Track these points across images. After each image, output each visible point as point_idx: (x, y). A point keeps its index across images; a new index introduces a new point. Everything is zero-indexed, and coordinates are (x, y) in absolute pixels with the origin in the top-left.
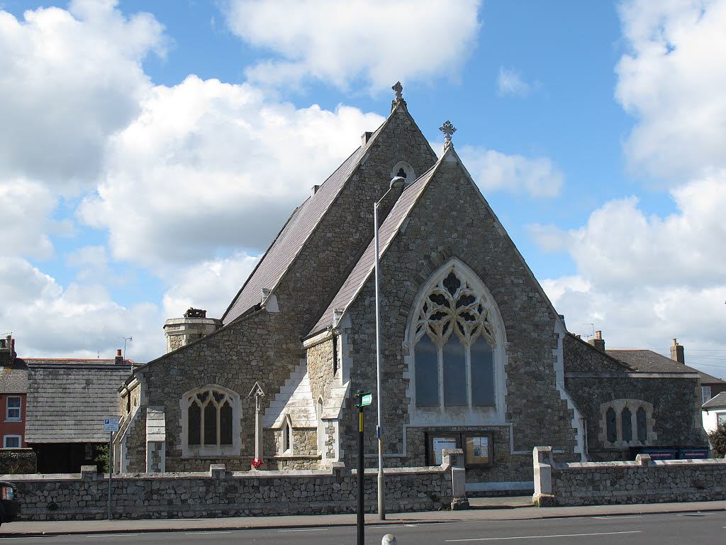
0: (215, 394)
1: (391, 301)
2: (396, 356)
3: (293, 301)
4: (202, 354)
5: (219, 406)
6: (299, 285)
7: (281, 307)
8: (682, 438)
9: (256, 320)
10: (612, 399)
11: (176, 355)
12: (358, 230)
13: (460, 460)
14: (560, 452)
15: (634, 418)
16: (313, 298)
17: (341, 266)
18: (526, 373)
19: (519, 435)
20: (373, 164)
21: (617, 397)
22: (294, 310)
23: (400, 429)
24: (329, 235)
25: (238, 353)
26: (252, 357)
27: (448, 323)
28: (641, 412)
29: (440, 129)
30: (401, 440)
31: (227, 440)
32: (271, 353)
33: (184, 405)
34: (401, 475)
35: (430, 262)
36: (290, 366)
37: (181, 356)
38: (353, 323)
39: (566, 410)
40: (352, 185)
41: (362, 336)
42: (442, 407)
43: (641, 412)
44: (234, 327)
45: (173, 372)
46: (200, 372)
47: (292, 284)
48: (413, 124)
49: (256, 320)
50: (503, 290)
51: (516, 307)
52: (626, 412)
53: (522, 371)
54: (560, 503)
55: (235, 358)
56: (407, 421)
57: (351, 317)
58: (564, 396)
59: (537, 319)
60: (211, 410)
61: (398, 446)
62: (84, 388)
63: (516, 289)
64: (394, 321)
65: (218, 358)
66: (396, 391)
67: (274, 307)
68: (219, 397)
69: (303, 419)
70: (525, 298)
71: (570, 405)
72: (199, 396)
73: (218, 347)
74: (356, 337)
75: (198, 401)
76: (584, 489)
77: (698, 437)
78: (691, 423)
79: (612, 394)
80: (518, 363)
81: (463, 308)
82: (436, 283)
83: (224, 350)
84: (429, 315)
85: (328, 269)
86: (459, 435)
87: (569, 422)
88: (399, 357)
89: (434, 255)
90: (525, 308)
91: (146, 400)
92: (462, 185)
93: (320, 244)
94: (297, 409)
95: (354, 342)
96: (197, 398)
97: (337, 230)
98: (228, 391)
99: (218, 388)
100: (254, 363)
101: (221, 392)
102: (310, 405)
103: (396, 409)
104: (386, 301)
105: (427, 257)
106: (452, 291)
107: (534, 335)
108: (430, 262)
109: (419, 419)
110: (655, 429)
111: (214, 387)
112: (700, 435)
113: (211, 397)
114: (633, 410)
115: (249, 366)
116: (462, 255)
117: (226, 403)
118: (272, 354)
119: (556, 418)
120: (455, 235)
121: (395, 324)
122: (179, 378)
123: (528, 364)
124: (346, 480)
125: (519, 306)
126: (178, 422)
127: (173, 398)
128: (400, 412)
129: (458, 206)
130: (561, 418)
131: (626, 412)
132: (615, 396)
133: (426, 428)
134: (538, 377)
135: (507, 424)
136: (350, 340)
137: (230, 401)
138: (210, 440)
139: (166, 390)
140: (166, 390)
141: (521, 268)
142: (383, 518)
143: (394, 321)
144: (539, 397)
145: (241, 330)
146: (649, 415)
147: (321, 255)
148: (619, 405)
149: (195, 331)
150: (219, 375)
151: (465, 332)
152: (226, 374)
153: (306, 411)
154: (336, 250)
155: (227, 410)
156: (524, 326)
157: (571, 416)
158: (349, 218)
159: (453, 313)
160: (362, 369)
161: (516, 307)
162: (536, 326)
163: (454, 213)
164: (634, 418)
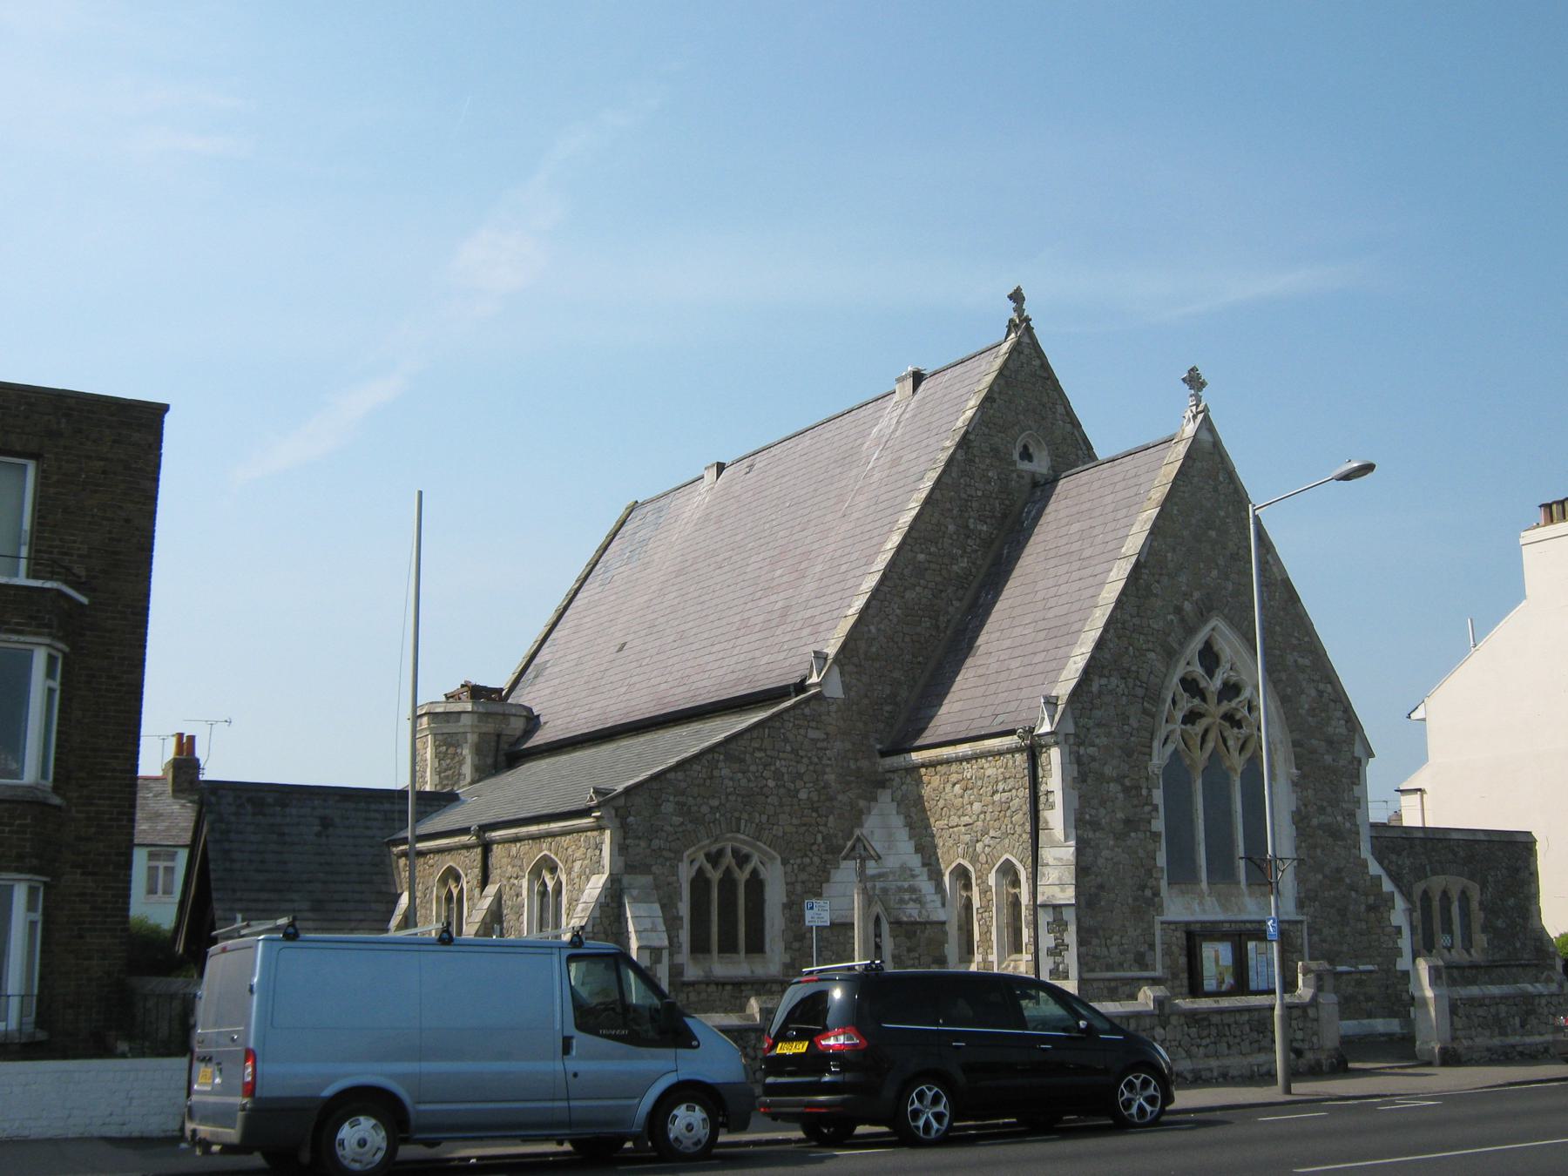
0: (735, 852)
1: (1131, 685)
2: (1141, 788)
3: (865, 679)
4: (716, 773)
5: (742, 876)
6: (874, 649)
7: (846, 687)
8: (1518, 945)
9: (807, 711)
10: (1426, 877)
11: (671, 776)
12: (965, 551)
13: (1329, 982)
14: (1370, 967)
15: (1436, 904)
16: (896, 674)
17: (941, 618)
18: (1320, 826)
19: (1316, 938)
20: (987, 431)
21: (1435, 873)
22: (866, 696)
23: (1151, 926)
24: (921, 557)
25: (778, 775)
26: (799, 784)
27: (1206, 731)
28: (1464, 896)
29: (1184, 380)
30: (1152, 946)
31: (756, 945)
32: (831, 777)
33: (686, 873)
34: (1249, 1010)
35: (1182, 620)
36: (862, 803)
37: (680, 775)
38: (1076, 724)
39: (1379, 894)
40: (955, 469)
41: (1091, 750)
42: (1204, 885)
43: (1464, 896)
44: (770, 724)
45: (668, 808)
46: (713, 810)
47: (862, 645)
48: (1045, 366)
49: (807, 711)
50: (1284, 676)
51: (1303, 708)
52: (1445, 894)
53: (1315, 822)
54: (1463, 1059)
55: (771, 783)
56: (1159, 909)
57: (1073, 713)
58: (1374, 868)
59: (1330, 730)
60: (728, 882)
61: (1148, 959)
62: (318, 835)
63: (1301, 676)
64: (1135, 725)
65: (744, 782)
66: (1141, 853)
67: (835, 690)
68: (742, 859)
69: (911, 905)
70: (1313, 693)
71: (1387, 886)
72: (708, 856)
73: (742, 761)
74: (1082, 751)
75: (708, 867)
76: (1487, 1033)
77: (1538, 944)
78: (1528, 918)
79: (1428, 868)
80: (1309, 807)
81: (1226, 706)
82: (1189, 663)
83: (753, 768)
84: (1179, 715)
85: (920, 621)
86: (1237, 938)
87: (1385, 915)
88: (1144, 792)
89: (1187, 606)
90: (1314, 709)
91: (620, 862)
92: (1221, 483)
93: (906, 572)
94: (893, 886)
95: (1079, 761)
96: (705, 861)
97: (933, 549)
98: (759, 849)
99: (744, 842)
100: (803, 795)
101: (746, 849)
102: (920, 878)
103: (1143, 888)
104: (1123, 685)
105: (1178, 610)
106: (1210, 673)
107: (1328, 758)
108: (1182, 620)
109: (1179, 908)
110: (1484, 930)
111: (736, 839)
112: (1542, 943)
113: (728, 859)
114: (1455, 895)
115: (795, 800)
116: (1226, 611)
117: (755, 873)
118: (833, 777)
119: (1363, 908)
120: (1215, 573)
121: (1137, 730)
122: (677, 820)
123: (1322, 810)
124: (1174, 1020)
125: (1306, 706)
126: (676, 908)
127: (666, 859)
128: (1148, 893)
129: (1217, 521)
130: (1370, 908)
131: (1445, 894)
132: (1431, 870)
133: (1187, 923)
134: (1335, 833)
135: (1300, 918)
136: (1072, 756)
137: (761, 868)
138: (728, 946)
139: (656, 843)
140: (656, 843)
141: (1306, 639)
142: (1288, 1091)
143: (1135, 725)
144: (1339, 870)
145: (782, 731)
146: (1475, 905)
147: (908, 595)
148: (1437, 883)
149: (489, 727)
150: (745, 816)
151: (1231, 750)
152: (757, 815)
153: (913, 890)
154: (932, 585)
155: (756, 885)
156: (1314, 742)
157: (1390, 904)
158: (951, 528)
159: (1215, 710)
160: (1093, 812)
161: (1303, 708)
162: (1330, 742)
163: (1213, 534)
164: (1436, 904)
